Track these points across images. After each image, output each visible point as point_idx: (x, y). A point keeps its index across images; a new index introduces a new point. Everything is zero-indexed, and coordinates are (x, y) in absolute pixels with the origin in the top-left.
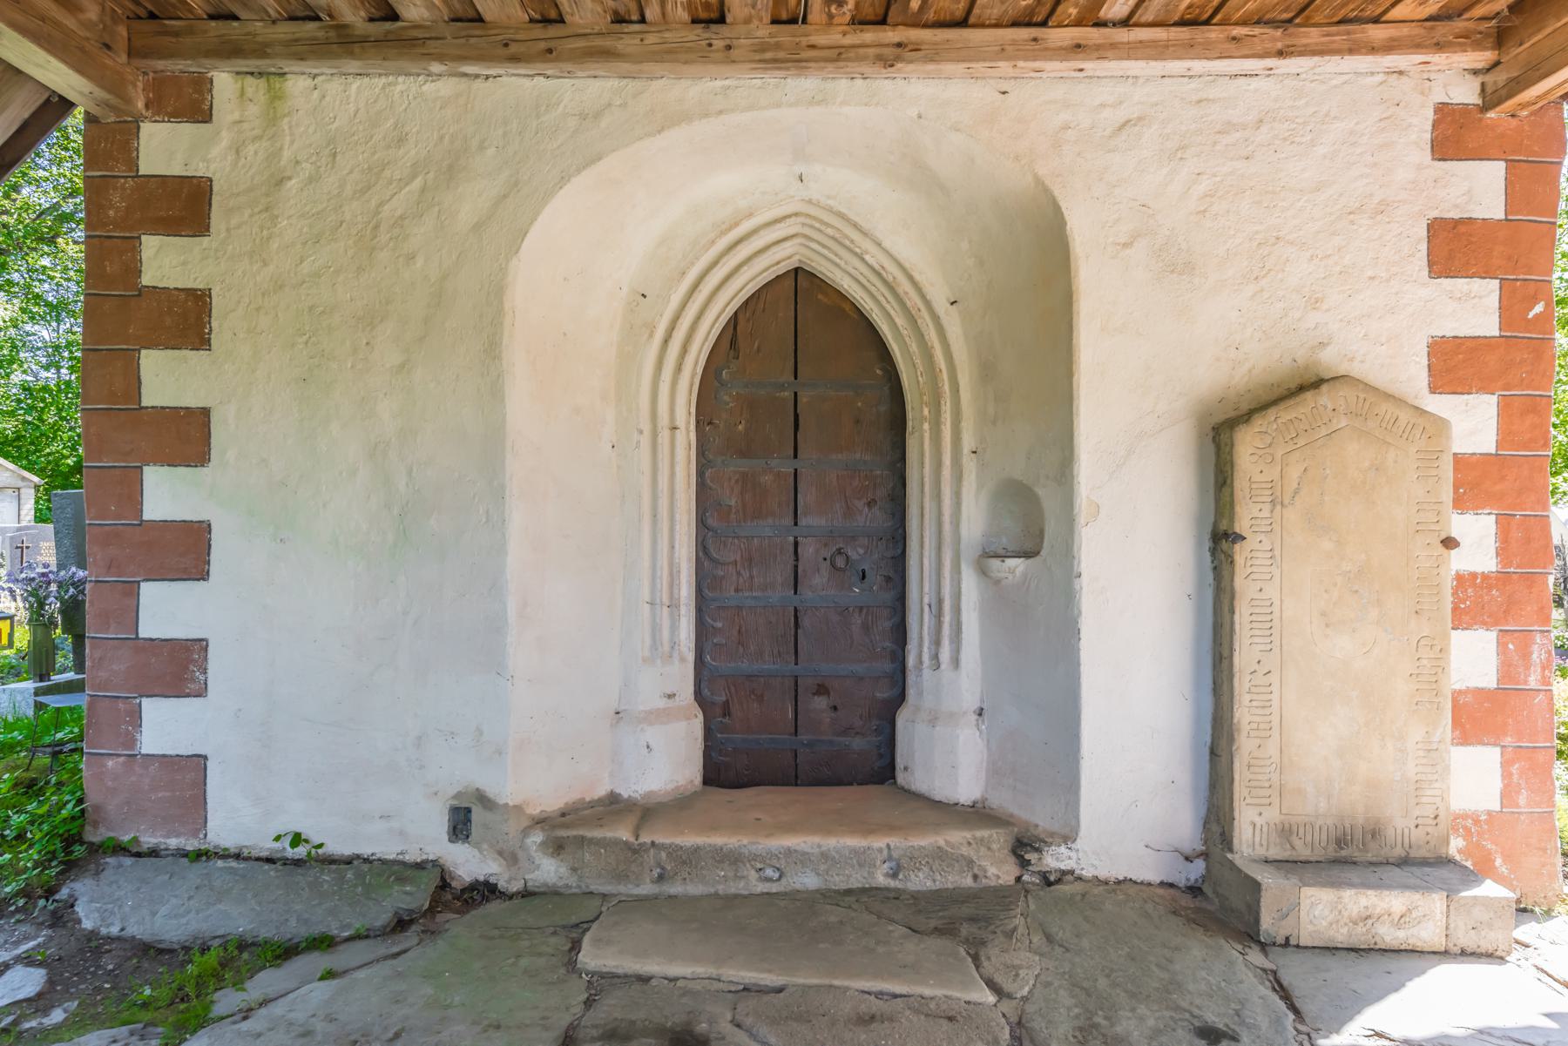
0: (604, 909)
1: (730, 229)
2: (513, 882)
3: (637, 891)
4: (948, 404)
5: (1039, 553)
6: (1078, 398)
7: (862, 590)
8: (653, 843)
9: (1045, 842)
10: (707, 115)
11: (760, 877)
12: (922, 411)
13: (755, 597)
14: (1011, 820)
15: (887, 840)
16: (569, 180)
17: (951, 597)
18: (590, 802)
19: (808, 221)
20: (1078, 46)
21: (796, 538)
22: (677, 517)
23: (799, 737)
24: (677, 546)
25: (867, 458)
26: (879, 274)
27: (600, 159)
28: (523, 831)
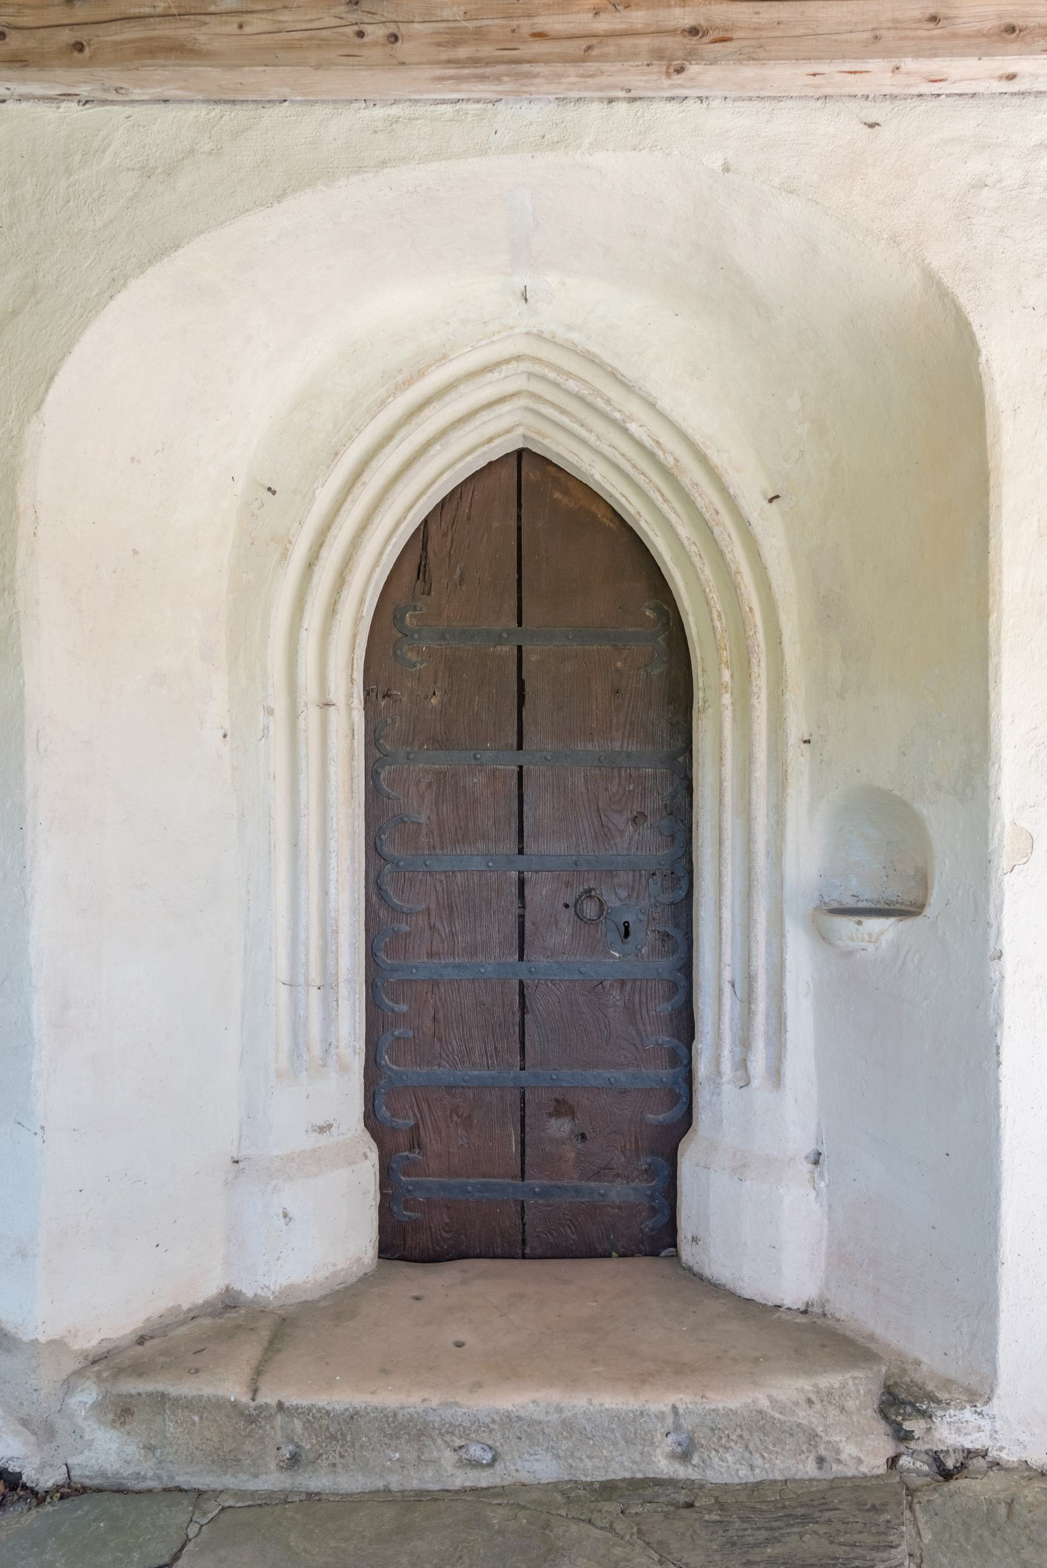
0: (193, 1531)
1: (409, 382)
2: (47, 1470)
3: (252, 1485)
4: (763, 664)
5: (922, 906)
6: (999, 653)
7: (624, 955)
8: (280, 1405)
9: (939, 1402)
10: (359, 169)
11: (460, 1459)
12: (720, 676)
13: (459, 966)
14: (872, 1346)
15: (672, 1398)
16: (125, 284)
17: (767, 973)
18: (190, 1310)
19: (537, 369)
20: (1011, 29)
21: (521, 873)
22: (333, 845)
23: (527, 1182)
24: (332, 890)
25: (633, 748)
26: (651, 455)
27: (177, 247)
28: (66, 1381)
